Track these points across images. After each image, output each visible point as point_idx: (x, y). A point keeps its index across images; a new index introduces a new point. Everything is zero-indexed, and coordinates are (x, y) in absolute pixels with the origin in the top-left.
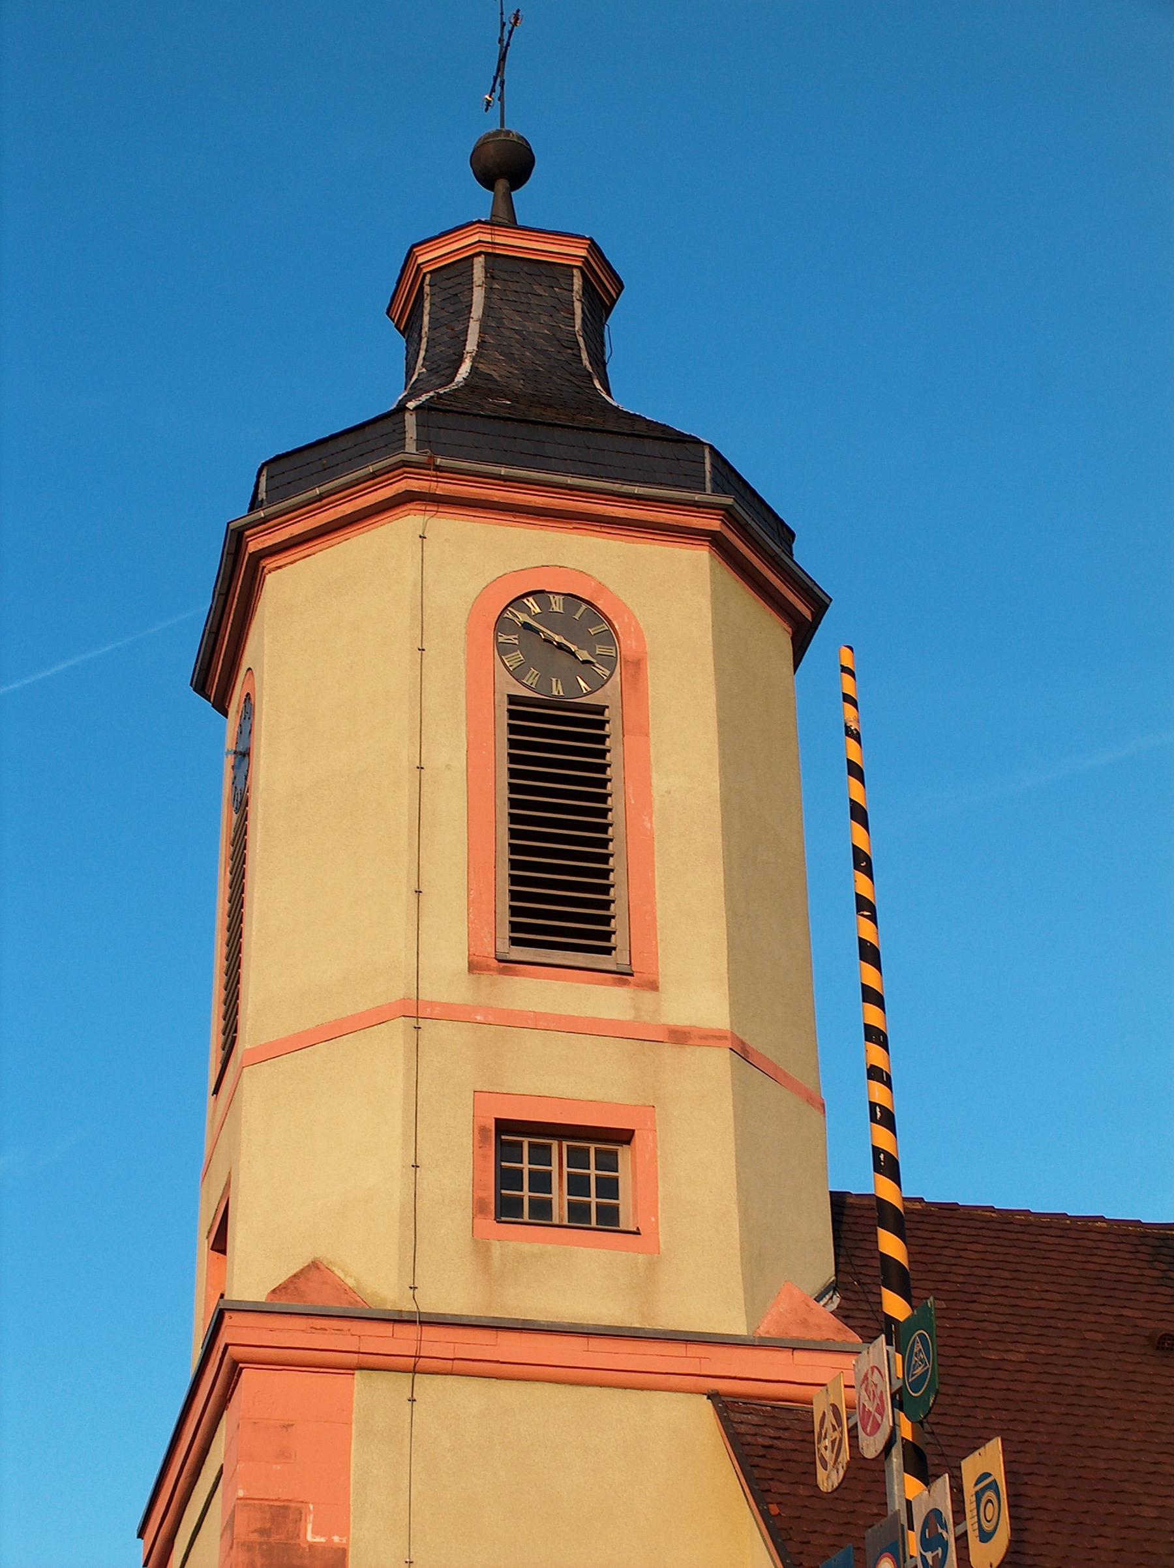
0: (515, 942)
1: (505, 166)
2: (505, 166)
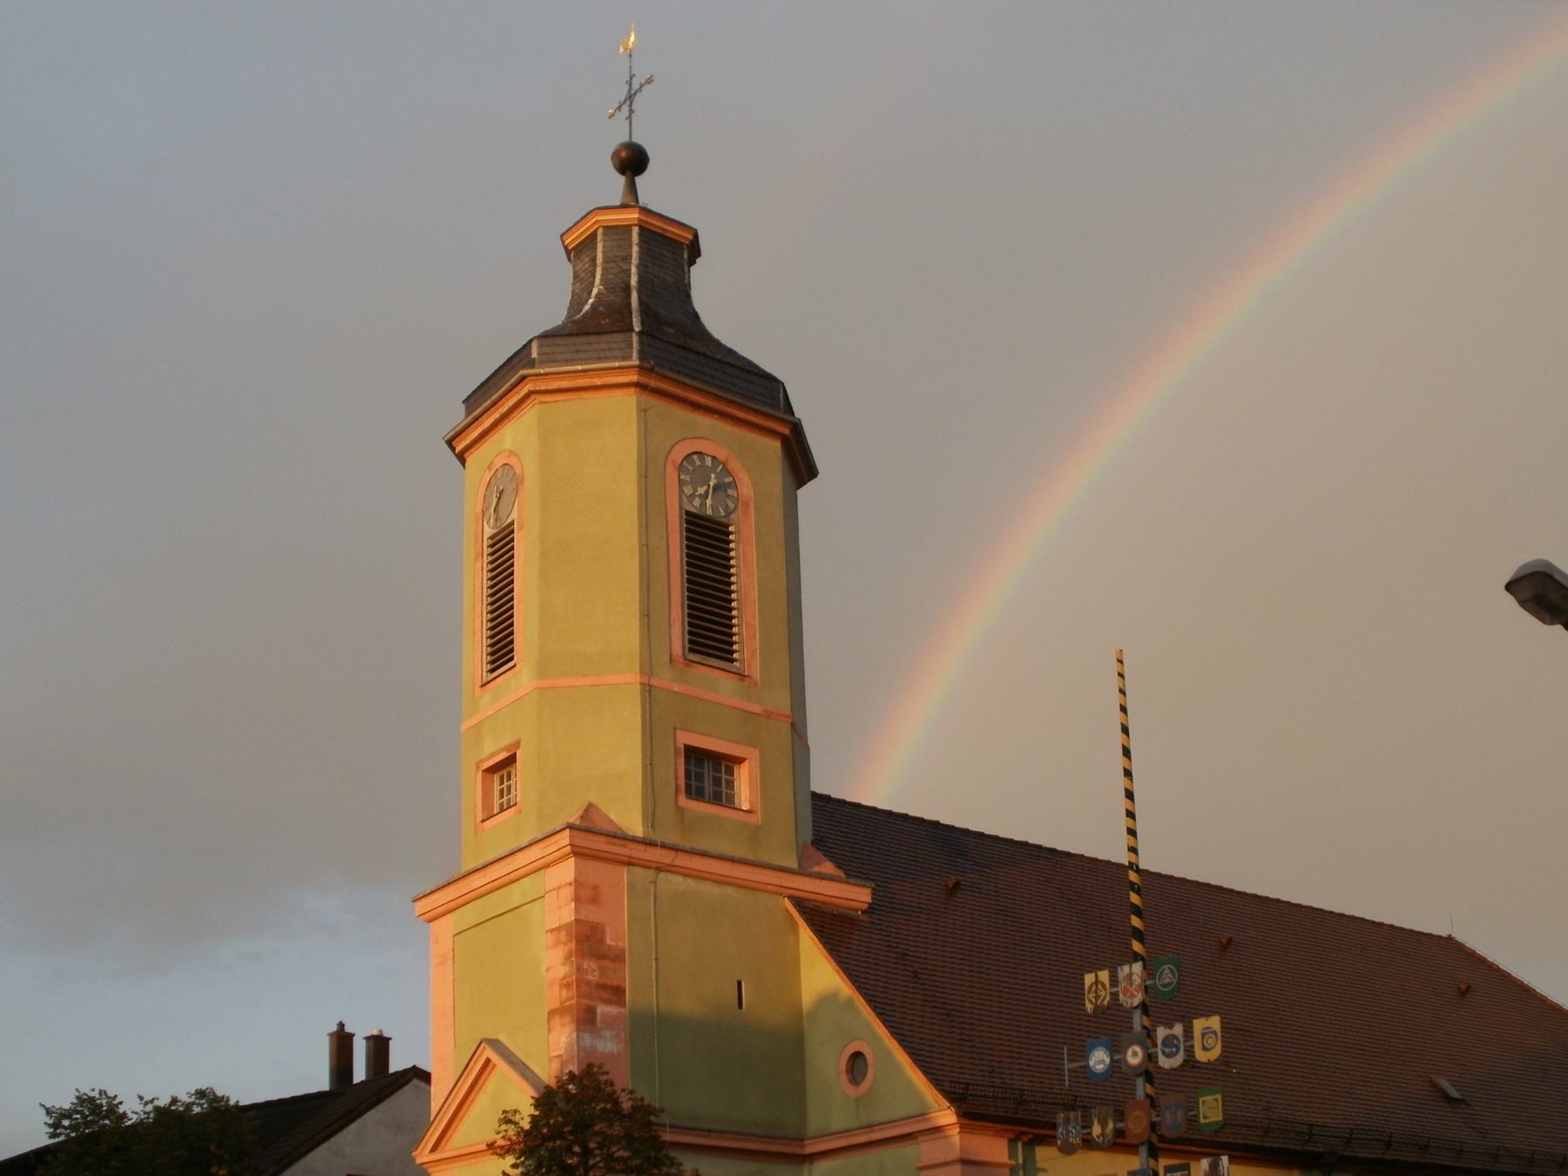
0: (492, 671)
1: (633, 162)
2: (633, 162)
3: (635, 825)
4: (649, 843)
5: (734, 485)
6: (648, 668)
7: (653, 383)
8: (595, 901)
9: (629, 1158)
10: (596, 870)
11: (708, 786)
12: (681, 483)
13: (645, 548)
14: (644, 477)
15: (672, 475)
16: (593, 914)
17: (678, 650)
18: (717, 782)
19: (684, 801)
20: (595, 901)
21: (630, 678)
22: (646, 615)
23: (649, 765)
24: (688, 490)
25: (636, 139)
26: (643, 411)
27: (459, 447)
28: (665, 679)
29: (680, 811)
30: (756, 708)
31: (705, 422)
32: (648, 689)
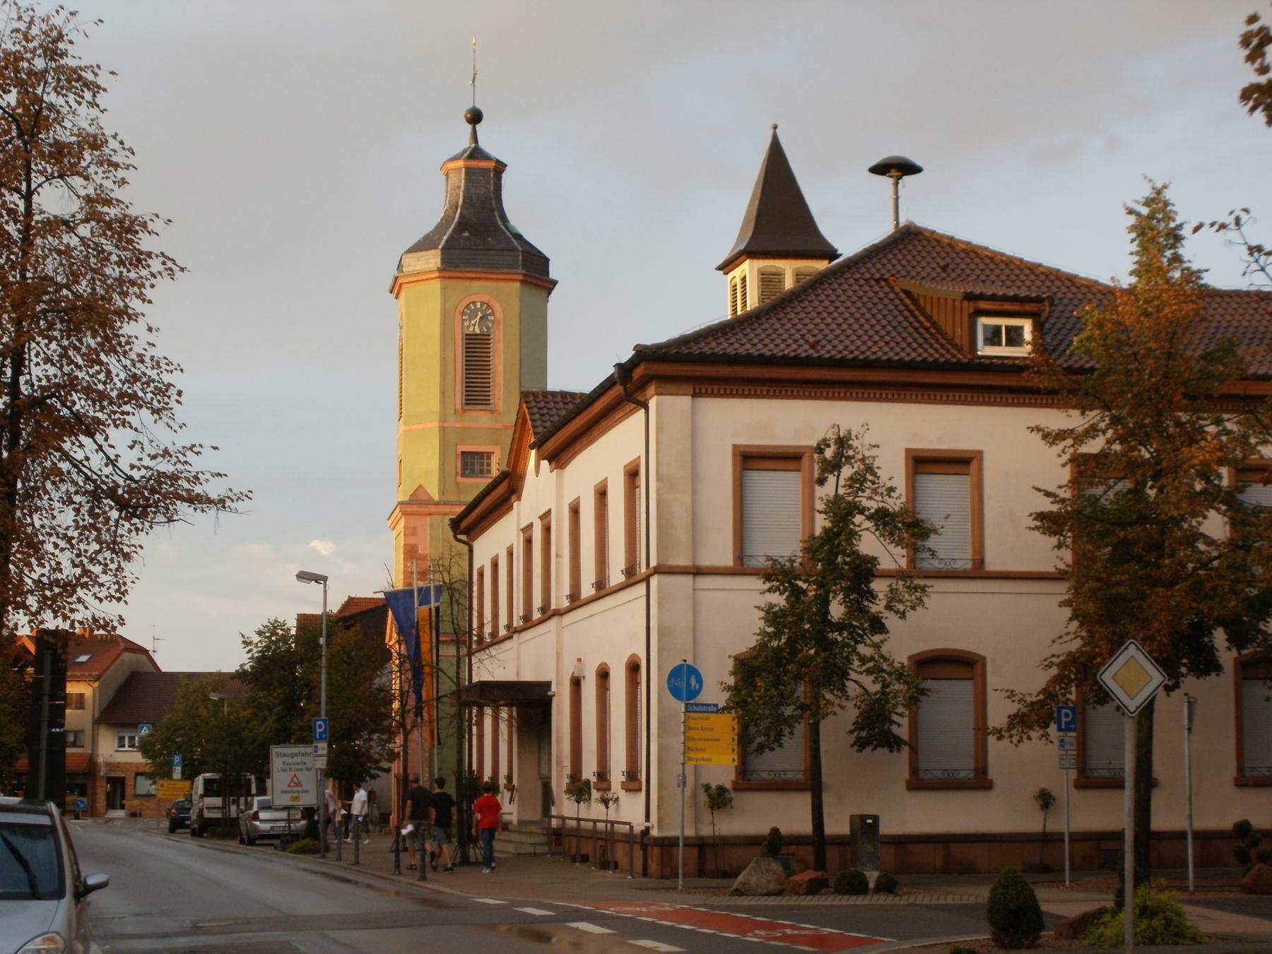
3: (436, 496)
4: (445, 504)
5: (493, 314)
6: (443, 420)
7: (446, 274)
8: (414, 534)
9: (15, 242)
10: (415, 521)
11: (477, 468)
12: (463, 321)
13: (443, 360)
14: (444, 324)
15: (458, 318)
16: (412, 540)
17: (459, 406)
18: (482, 464)
19: (459, 479)
20: (414, 534)
21: (435, 425)
22: (443, 393)
23: (443, 465)
24: (466, 324)
25: (479, 106)
26: (444, 289)
27: (726, 267)
28: (453, 422)
29: (457, 484)
30: (499, 426)
31: (476, 285)
32: (443, 429)
